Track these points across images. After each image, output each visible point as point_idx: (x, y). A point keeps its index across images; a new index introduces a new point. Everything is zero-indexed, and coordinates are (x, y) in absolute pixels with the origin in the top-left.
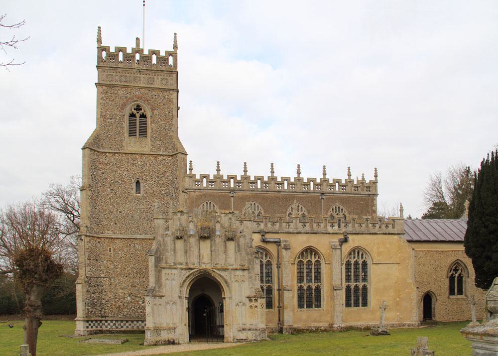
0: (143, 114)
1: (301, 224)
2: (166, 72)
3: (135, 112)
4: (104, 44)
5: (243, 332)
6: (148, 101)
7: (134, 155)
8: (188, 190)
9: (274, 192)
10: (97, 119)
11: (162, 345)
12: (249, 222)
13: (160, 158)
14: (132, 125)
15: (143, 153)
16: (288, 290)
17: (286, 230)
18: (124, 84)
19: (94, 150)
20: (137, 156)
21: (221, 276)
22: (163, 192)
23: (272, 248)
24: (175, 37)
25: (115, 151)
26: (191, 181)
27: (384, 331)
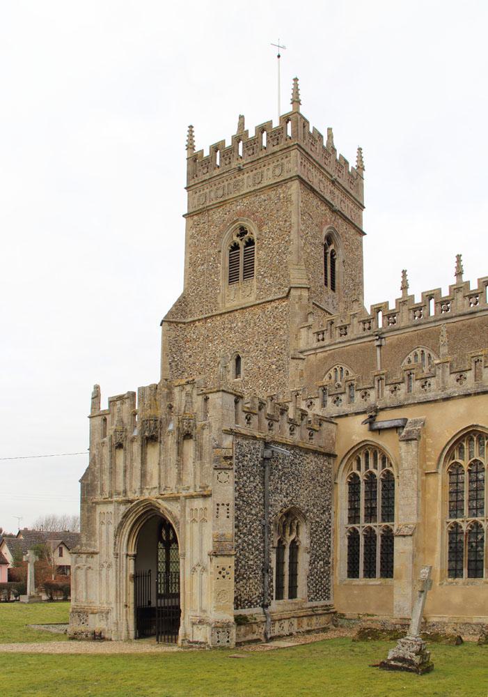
0: (250, 239)
1: (454, 376)
2: (280, 153)
3: (237, 240)
4: (197, 149)
5: (200, 627)
6: (254, 214)
7: (232, 314)
8: (306, 354)
9: (460, 316)
10: (185, 271)
11: (87, 639)
12: (218, 394)
13: (269, 307)
14: (233, 263)
15: (243, 306)
16: (404, 536)
17: (421, 397)
18: (221, 199)
19: (175, 322)
20: (237, 314)
21: (171, 510)
22: (274, 367)
23: (387, 443)
24: (296, 85)
25: (206, 316)
26: (311, 335)
27: (403, 660)
